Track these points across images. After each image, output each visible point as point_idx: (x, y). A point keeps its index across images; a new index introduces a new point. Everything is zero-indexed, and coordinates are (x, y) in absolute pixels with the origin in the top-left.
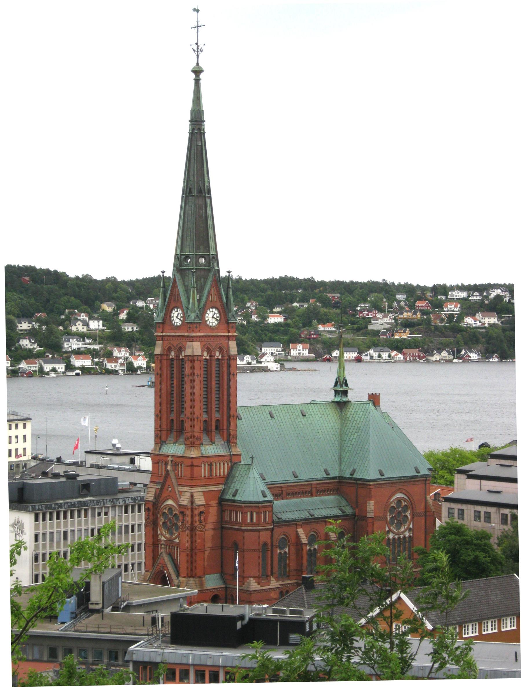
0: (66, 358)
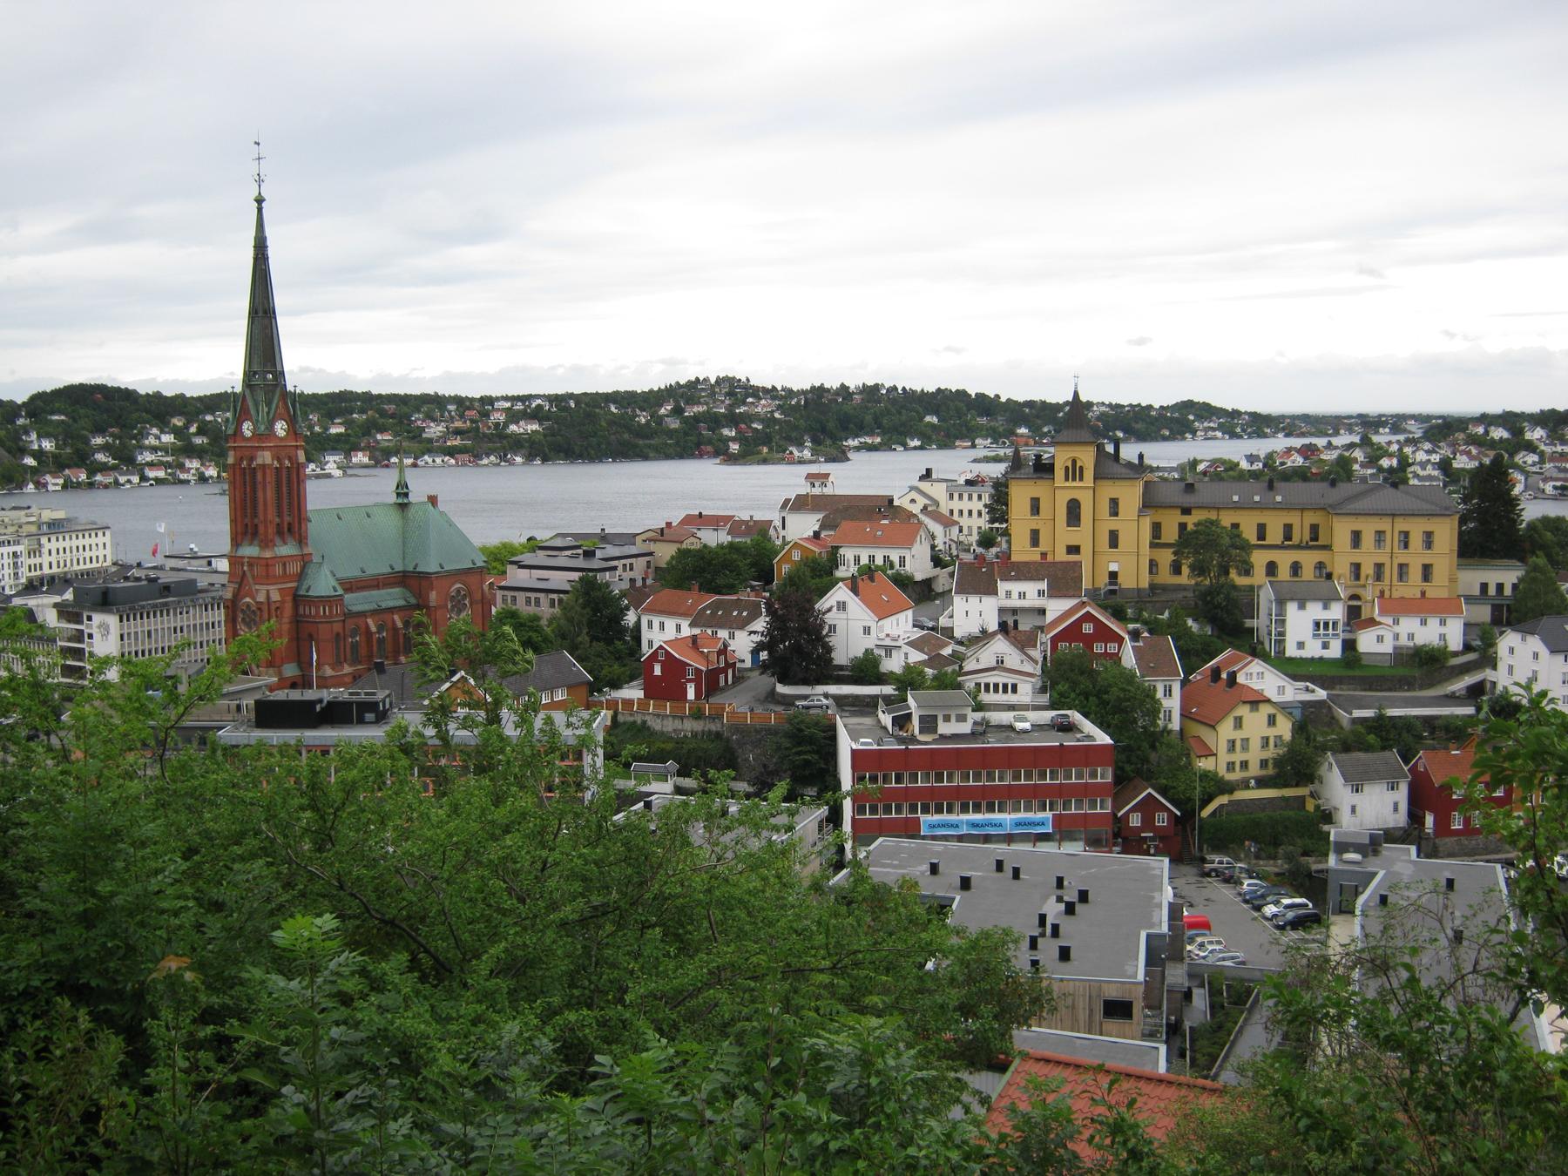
0: (140, 470)
